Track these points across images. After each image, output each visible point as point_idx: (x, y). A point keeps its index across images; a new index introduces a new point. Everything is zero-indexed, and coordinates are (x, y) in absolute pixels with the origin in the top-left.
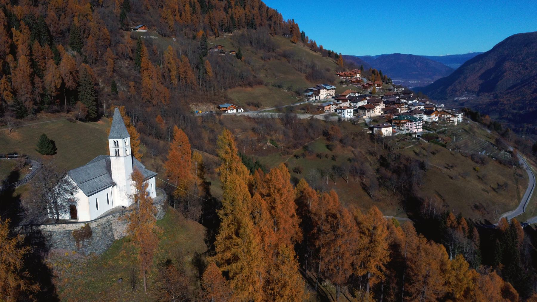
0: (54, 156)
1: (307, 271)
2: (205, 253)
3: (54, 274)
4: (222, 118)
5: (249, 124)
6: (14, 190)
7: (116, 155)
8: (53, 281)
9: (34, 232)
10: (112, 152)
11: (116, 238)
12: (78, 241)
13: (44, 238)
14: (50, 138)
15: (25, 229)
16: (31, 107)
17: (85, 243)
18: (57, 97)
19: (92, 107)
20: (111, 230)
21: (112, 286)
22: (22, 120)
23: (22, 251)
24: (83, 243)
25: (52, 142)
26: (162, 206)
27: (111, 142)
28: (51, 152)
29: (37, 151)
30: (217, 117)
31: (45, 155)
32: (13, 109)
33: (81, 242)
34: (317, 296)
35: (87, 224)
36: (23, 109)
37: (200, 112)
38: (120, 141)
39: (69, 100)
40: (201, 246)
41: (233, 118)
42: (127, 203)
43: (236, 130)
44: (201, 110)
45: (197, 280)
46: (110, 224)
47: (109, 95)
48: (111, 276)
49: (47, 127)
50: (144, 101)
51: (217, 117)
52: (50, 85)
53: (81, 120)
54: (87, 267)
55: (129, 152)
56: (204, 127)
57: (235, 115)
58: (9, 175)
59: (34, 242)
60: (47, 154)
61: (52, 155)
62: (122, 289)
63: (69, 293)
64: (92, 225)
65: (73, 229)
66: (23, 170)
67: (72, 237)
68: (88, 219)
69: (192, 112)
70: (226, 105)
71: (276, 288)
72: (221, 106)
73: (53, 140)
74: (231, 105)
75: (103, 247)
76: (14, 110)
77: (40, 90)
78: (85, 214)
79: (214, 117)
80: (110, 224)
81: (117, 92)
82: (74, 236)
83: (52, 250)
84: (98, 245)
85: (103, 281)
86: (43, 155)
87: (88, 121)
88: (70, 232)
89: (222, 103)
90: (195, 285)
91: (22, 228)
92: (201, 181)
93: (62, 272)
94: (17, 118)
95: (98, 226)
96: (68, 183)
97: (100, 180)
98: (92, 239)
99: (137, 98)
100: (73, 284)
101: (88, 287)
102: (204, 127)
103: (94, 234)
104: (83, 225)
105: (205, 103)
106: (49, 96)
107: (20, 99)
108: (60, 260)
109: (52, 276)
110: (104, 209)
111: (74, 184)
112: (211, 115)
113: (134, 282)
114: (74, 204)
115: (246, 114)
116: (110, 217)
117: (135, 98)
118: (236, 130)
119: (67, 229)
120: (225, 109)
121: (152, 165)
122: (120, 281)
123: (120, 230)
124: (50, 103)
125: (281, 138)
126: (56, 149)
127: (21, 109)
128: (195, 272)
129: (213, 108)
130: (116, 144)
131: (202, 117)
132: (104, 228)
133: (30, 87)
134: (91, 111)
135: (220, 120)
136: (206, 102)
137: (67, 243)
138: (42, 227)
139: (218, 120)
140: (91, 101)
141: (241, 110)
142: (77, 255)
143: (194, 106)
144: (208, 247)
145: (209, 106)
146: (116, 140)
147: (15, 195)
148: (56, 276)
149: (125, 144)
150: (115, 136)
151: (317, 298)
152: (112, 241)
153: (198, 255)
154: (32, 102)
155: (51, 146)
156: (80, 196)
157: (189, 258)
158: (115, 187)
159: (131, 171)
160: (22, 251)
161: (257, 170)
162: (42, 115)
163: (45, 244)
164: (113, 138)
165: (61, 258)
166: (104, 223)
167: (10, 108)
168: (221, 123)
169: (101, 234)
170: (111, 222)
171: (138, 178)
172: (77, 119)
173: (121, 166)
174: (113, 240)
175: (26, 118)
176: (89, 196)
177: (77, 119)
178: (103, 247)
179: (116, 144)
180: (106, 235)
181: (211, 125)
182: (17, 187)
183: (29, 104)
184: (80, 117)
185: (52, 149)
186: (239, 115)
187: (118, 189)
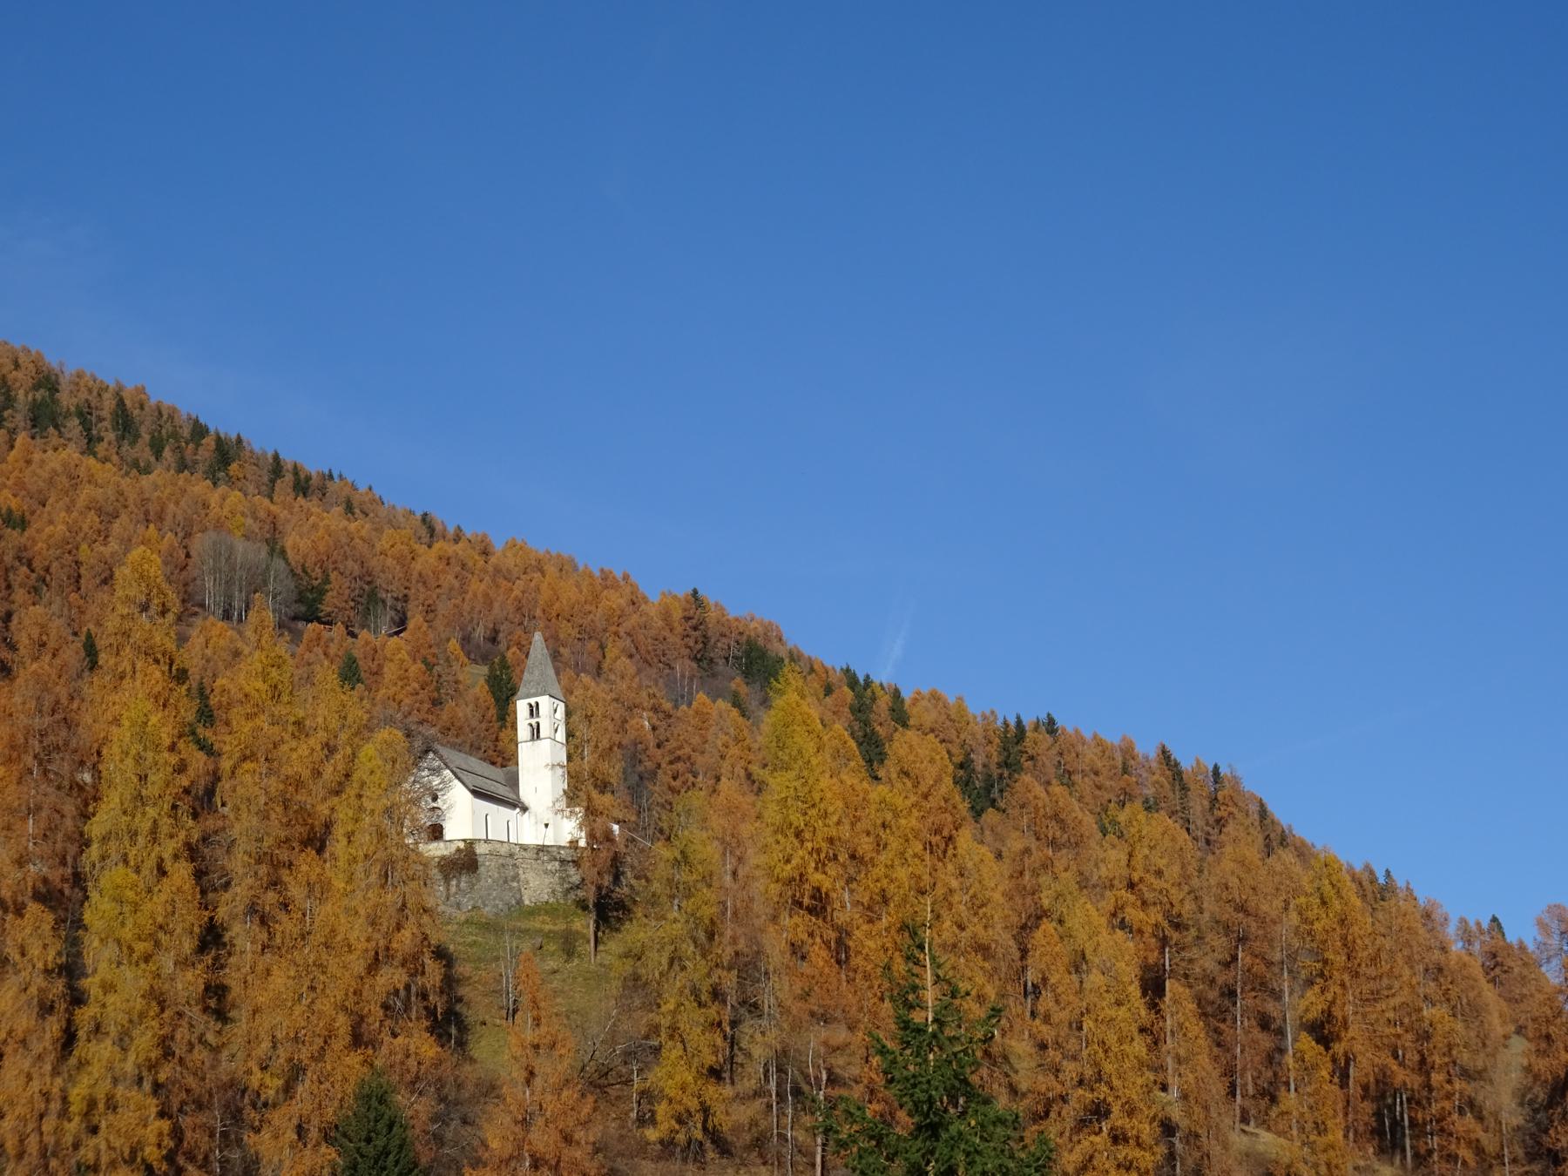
10: (523, 732)
17: (463, 885)
24: (458, 886)
27: (522, 707)
33: (454, 882)
35: (470, 844)
55: (561, 736)
64: (481, 849)
65: (439, 853)
71: (948, 965)
98: (479, 880)
103: (482, 869)
104: (462, 845)
125: (1190, 1161)
130: (534, 711)
146: (532, 701)
149: (551, 711)
173: (540, 764)
179: (534, 711)
187: (533, 819)
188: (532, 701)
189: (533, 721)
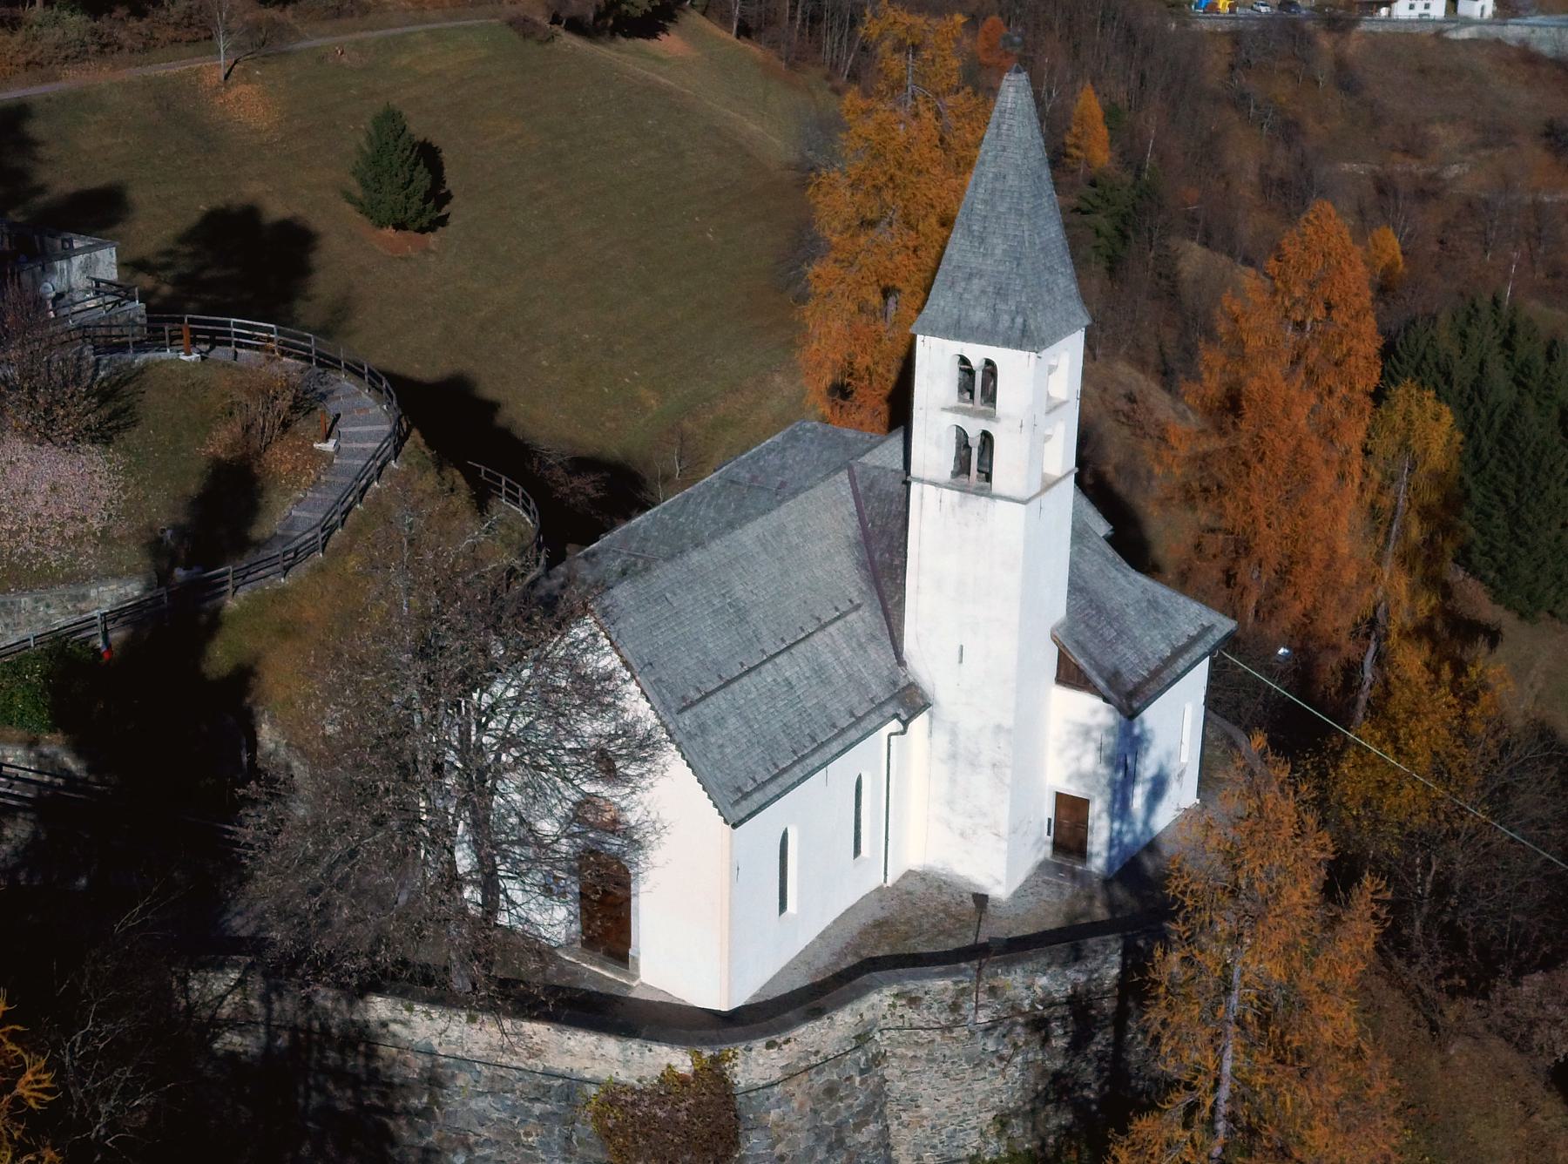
0: (431, 238)
4: (1353, 46)
5: (1528, 102)
6: (215, 622)
7: (962, 467)
13: (388, 1087)
14: (419, 128)
15: (265, 1000)
25: (429, 155)
27: (936, 361)
28: (420, 213)
29: (349, 197)
30: (1325, 42)
31: (389, 232)
43: (1438, 130)
46: (877, 1060)
49: (405, 59)
51: (1325, 42)
53: (576, 26)
56: (1240, 101)
57: (1438, 34)
58: (193, 487)
59: (316, 1099)
60: (397, 227)
61: (422, 230)
65: (599, 1070)
66: (280, 459)
67: (585, 1128)
73: (436, 140)
79: (1307, 40)
82: (607, 1135)
86: (381, 225)
87: (614, 31)
88: (571, 1086)
91: (240, 982)
92: (1426, 604)
95: (790, 1075)
96: (594, 693)
102: (1240, 101)
111: (637, 707)
114: (614, 844)
115: (1514, 31)
116: (878, 1002)
118: (1438, 130)
119: (560, 1064)
126: (448, 197)
130: (978, 385)
131: (1236, 37)
132: (831, 1091)
138: (380, 1008)
139: (1323, 70)
146: (977, 354)
147: (219, 658)
149: (1043, 390)
150: (979, 315)
155: (423, 179)
156: (670, 803)
158: (919, 724)
163: (393, 1140)
164: (957, 331)
166: (830, 1049)
168: (1346, 78)
172: (555, 20)
173: (991, 562)
176: (734, 826)
177: (555, 20)
179: (978, 385)
185: (425, 201)
186: (1465, 34)
187: (942, 739)
188: (977, 354)
189: (974, 428)
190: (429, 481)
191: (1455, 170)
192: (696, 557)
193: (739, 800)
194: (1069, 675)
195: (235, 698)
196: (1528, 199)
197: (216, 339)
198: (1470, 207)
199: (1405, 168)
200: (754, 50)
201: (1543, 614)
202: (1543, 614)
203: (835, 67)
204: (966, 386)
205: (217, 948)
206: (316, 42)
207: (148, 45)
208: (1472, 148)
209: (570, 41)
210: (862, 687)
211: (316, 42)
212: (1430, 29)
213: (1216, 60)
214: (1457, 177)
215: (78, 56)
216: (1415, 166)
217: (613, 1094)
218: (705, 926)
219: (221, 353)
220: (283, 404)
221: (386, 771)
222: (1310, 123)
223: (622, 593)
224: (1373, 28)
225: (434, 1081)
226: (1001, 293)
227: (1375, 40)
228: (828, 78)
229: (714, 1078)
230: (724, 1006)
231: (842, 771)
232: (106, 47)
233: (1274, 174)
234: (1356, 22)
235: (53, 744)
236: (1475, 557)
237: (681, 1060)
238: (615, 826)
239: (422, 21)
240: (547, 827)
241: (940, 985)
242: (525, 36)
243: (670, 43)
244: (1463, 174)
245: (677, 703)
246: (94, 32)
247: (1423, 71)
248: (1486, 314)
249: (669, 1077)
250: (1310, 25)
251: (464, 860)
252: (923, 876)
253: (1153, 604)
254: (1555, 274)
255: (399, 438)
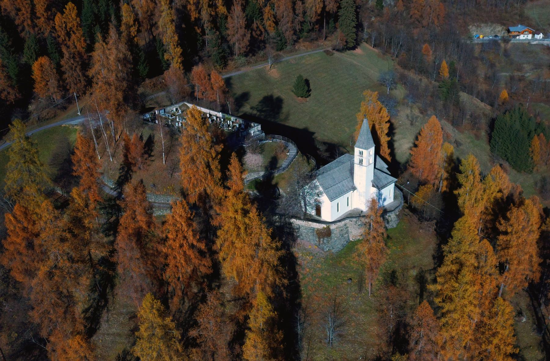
0: (308, 99)
1: (543, 307)
2: (430, 270)
3: (298, 262)
4: (509, 46)
6: (273, 178)
8: (298, 269)
9: (286, 223)
10: (356, 159)
11: (351, 240)
12: (319, 238)
13: (293, 229)
16: (291, 38)
17: (325, 241)
18: (317, 22)
19: (351, 34)
20: (347, 232)
21: (342, 284)
22: (281, 53)
23: (279, 253)
24: (323, 241)
25: (307, 82)
26: (397, 215)
27: (357, 150)
29: (293, 91)
30: (503, 45)
31: (300, 98)
32: (275, 41)
34: (541, 342)
36: (283, 40)
37: (481, 37)
38: (365, 152)
39: (328, 23)
40: (428, 262)
41: (525, 48)
42: (364, 207)
44: (482, 34)
45: (417, 297)
46: (347, 227)
47: (373, 11)
48: (343, 275)
49: (304, 61)
50: (412, 20)
51: (503, 45)
52: (311, 8)
53: (338, 50)
54: (325, 262)
56: (482, 59)
57: (529, 43)
62: (350, 289)
63: (309, 282)
64: (333, 227)
65: (317, 227)
67: (315, 233)
68: (329, 220)
69: (470, 38)
70: (520, 27)
72: (511, 29)
73: (309, 78)
74: (526, 29)
75: (339, 246)
76: (275, 43)
77: (300, 18)
78: (327, 215)
79: (499, 45)
80: (347, 227)
81: (382, 7)
82: (317, 234)
83: (299, 241)
84: (336, 244)
85: (336, 277)
88: (314, 229)
89: (514, 25)
90: (414, 301)
93: (305, 262)
94: (277, 50)
96: (316, 187)
97: (343, 185)
98: (331, 239)
99: (404, 14)
100: (312, 275)
101: (324, 280)
103: (333, 235)
105: (490, 24)
106: (309, 23)
107: (281, 30)
108: (304, 251)
109: (297, 264)
110: (344, 210)
111: (321, 189)
112: (494, 43)
113: (361, 284)
116: (347, 221)
117: (402, 15)
118: (525, 65)
119: (312, 226)
120: (516, 34)
121: (407, 116)
122: (349, 282)
123: (355, 232)
124: (309, 31)
126: (311, 90)
127: (281, 40)
128: (417, 288)
129: (500, 31)
130: (361, 153)
131: (482, 44)
132: (342, 230)
133: (291, 14)
134: (350, 40)
135: (506, 51)
136: (492, 22)
137: (311, 237)
138: (293, 220)
139: (502, 50)
140: (351, 28)
141: (540, 36)
142: (318, 250)
143: (474, 28)
144: (435, 264)
145: (495, 28)
146: (361, 150)
147: (274, 182)
148: (300, 265)
151: (540, 344)
152: (347, 242)
153: (423, 271)
154: (292, 32)
156: (324, 199)
157: (414, 273)
158: (355, 191)
159: (372, 177)
160: (279, 253)
161: (538, 135)
162: (302, 46)
164: (359, 147)
165: (305, 249)
167: (271, 40)
168: (506, 54)
169: (338, 235)
170: (348, 225)
171: (378, 185)
174: (349, 242)
175: (285, 50)
178: (339, 246)
179: (361, 153)
180: (343, 236)
181: (491, 56)
182: (276, 175)
183: (289, 35)
184: (337, 47)
186: (535, 43)
190: (301, 159)
191: (528, 74)
192: (329, 172)
193: (332, 199)
194: (373, 186)
195: (276, 186)
196: (543, 81)
197: (274, 138)
198: (531, 82)
199: (517, 74)
200: (376, 50)
201: (523, 171)
202: (523, 171)
203: (393, 54)
204: (360, 153)
205: (276, 214)
206: (287, 58)
207: (256, 62)
208: (533, 69)
209: (337, 54)
210: (348, 187)
211: (287, 58)
212: (527, 42)
213: (477, 50)
214: (529, 76)
215: (243, 65)
216: (520, 74)
217: (318, 230)
218: (329, 212)
219: (274, 140)
220: (283, 149)
221: (295, 197)
222: (497, 64)
223: (320, 176)
224: (515, 42)
225: (299, 229)
226: (363, 143)
227: (514, 44)
228: (392, 57)
229: (328, 228)
230: (330, 221)
231: (346, 196)
232: (249, 63)
233: (488, 75)
234: (510, 40)
235: (255, 192)
236: (509, 160)
237: (325, 226)
238: (320, 202)
239: (307, 52)
240: (311, 202)
241: (354, 219)
242: (328, 54)
243: (358, 51)
244: (530, 75)
245: (325, 189)
246: (247, 61)
247: (524, 52)
248: (517, 111)
249: (324, 228)
250: (500, 41)
251: (303, 205)
252: (356, 209)
253: (386, 177)
254: (548, 97)
255: (297, 152)
